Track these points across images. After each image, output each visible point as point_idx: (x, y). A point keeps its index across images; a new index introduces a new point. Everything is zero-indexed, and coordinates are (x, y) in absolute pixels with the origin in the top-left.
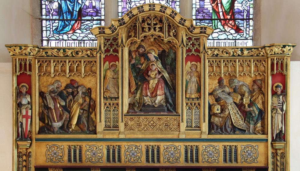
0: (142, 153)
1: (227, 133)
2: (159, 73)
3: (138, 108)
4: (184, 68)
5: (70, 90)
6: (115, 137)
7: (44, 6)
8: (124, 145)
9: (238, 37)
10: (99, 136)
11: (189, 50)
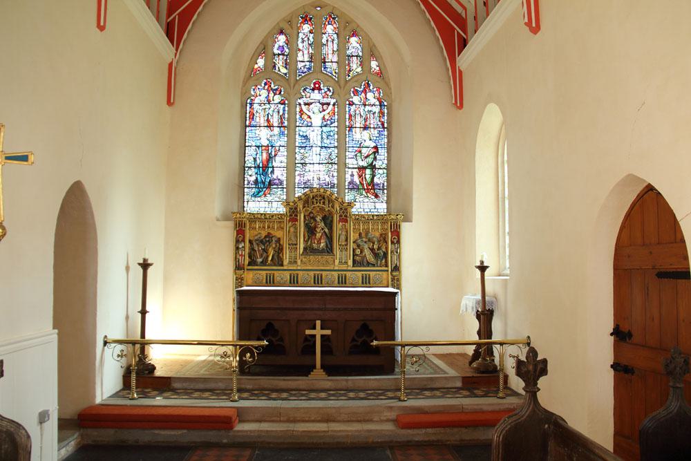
0: (311, 278)
1: (364, 266)
2: (323, 229)
3: (309, 250)
4: (338, 226)
5: (267, 239)
6: (295, 268)
7: (246, 179)
8: (301, 273)
9: (377, 201)
10: (285, 268)
11: (341, 216)
